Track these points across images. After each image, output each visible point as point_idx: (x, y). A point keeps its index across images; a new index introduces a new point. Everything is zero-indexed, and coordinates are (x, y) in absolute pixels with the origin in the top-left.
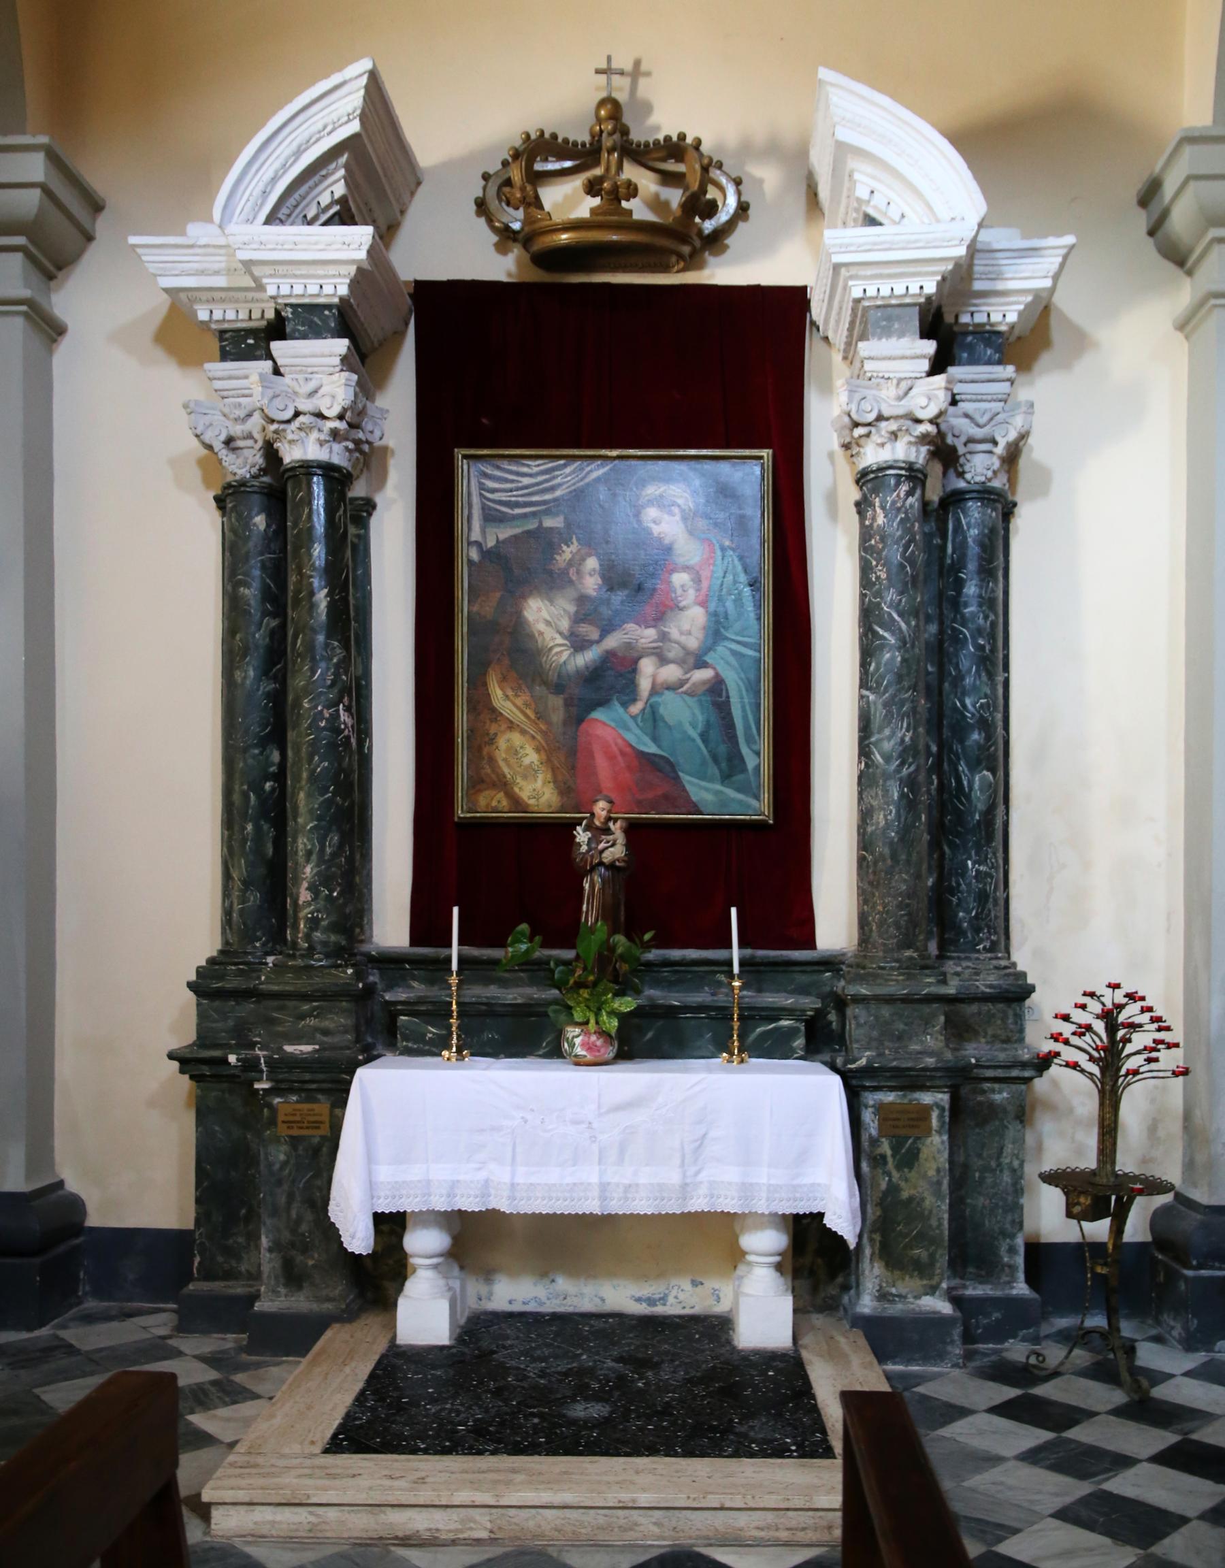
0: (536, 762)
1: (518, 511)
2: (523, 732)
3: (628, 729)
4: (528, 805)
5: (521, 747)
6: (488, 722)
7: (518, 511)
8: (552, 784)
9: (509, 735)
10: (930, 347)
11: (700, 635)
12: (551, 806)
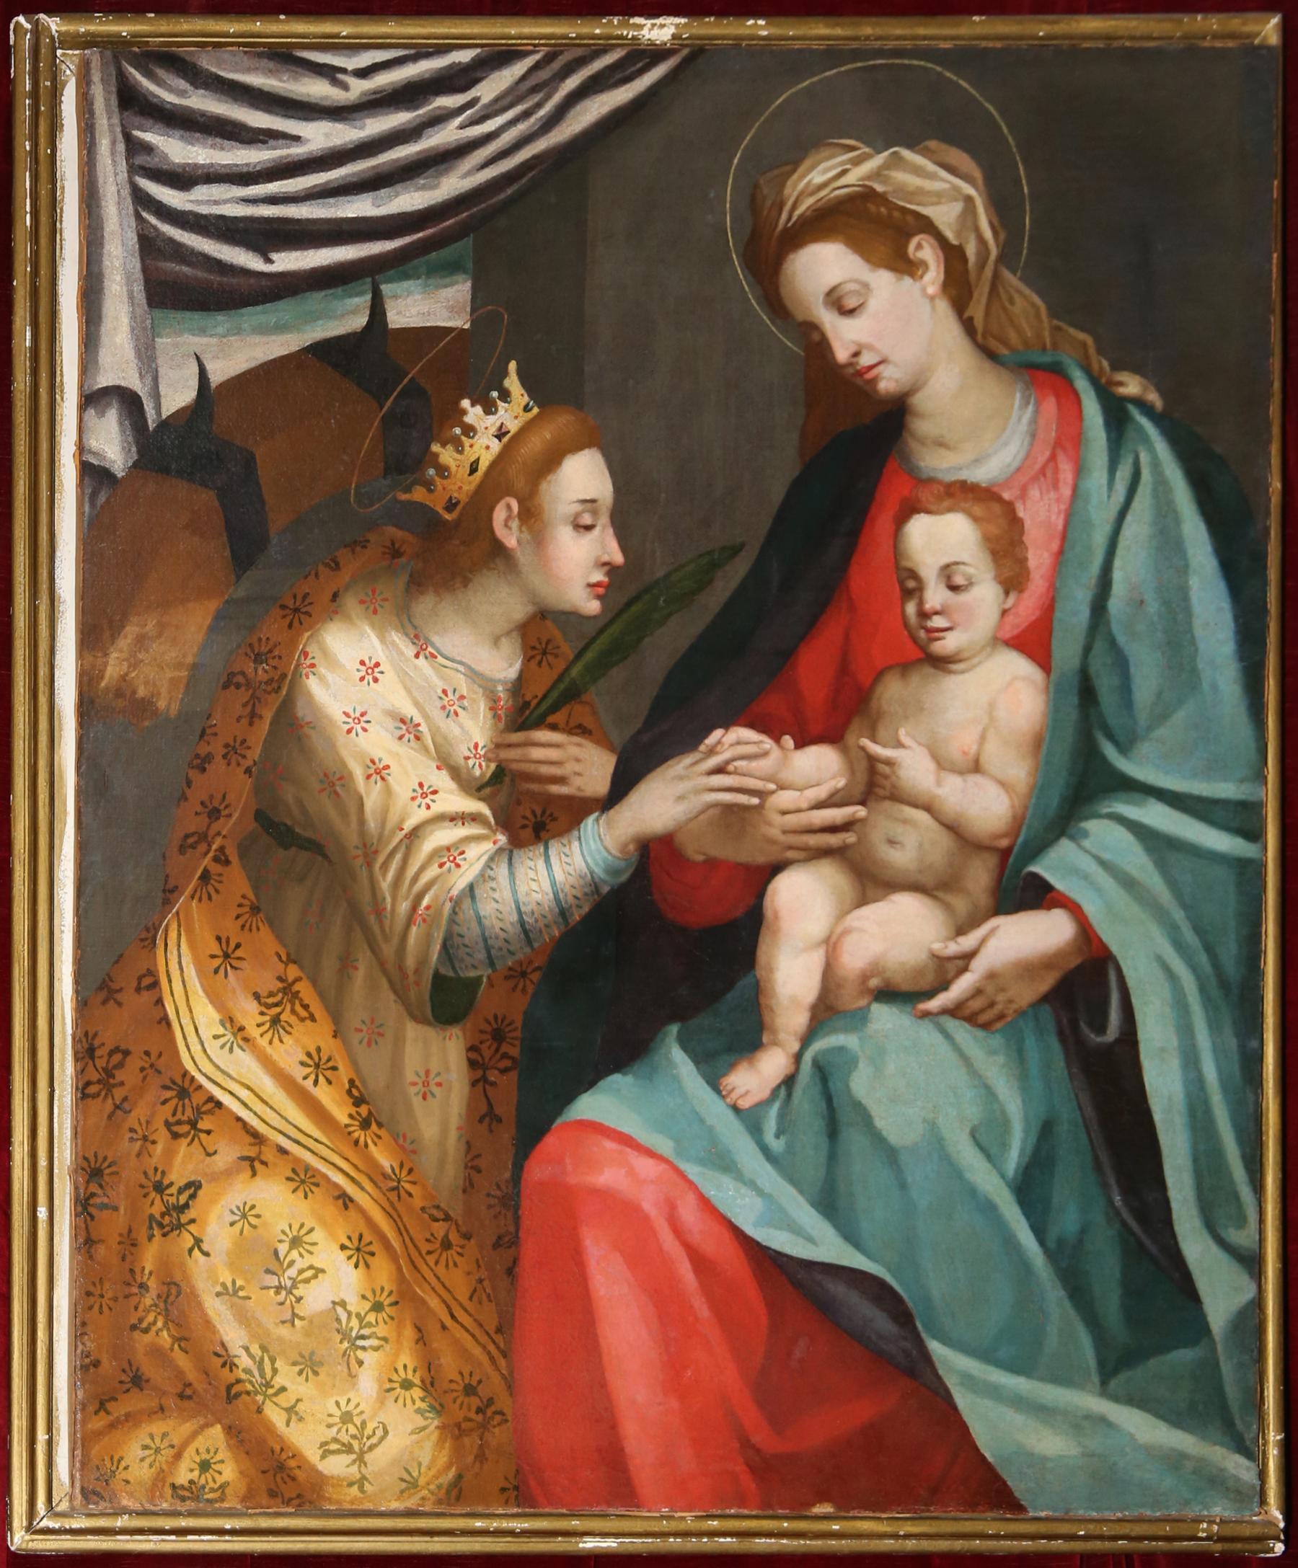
0: (355, 1305)
1: (288, 261)
2: (304, 1179)
3: (723, 1162)
4: (319, 1481)
5: (296, 1242)
6: (162, 1136)
7: (288, 261)
8: (417, 1393)
9: (243, 1191)
10: (320, 1275)
11: (1019, 771)
12: (413, 1485)
